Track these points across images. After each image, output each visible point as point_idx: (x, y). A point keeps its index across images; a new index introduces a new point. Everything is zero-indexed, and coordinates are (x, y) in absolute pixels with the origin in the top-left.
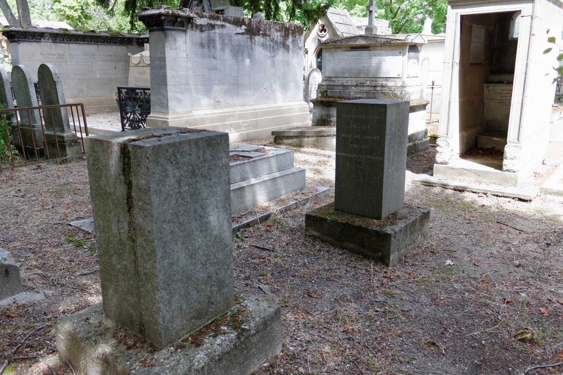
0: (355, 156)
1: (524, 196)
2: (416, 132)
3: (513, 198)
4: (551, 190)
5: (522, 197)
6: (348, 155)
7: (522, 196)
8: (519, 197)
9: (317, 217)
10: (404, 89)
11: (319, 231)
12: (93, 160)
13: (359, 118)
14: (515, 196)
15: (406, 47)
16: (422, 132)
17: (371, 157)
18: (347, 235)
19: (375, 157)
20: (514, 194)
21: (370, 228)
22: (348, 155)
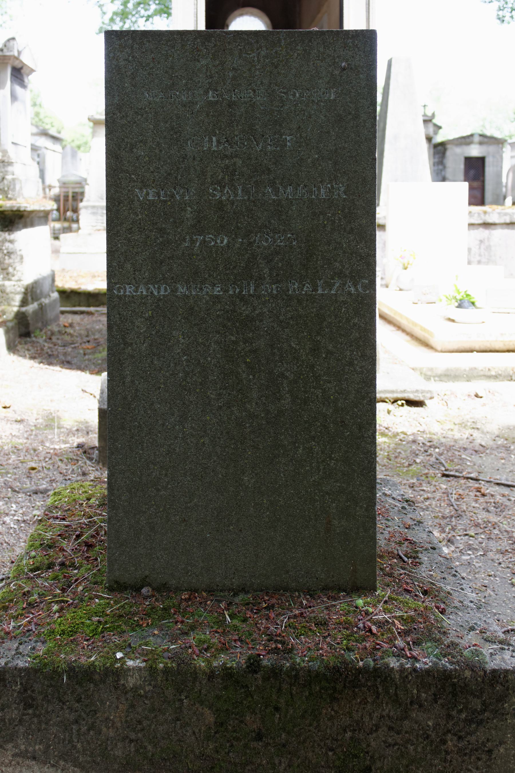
0: (217, 291)
1: (417, 391)
2: (39, 277)
3: (395, 401)
4: (431, 370)
5: (412, 397)
6: (182, 290)
7: (413, 392)
8: (406, 396)
9: (56, 673)
10: (10, 169)
11: (63, 756)
12: (310, 348)
13: (231, 104)
14: (396, 395)
15: (5, 68)
16: (48, 276)
17: (307, 288)
18: (259, 737)
19: (329, 285)
20: (392, 392)
21: (393, 663)
22: (182, 290)
